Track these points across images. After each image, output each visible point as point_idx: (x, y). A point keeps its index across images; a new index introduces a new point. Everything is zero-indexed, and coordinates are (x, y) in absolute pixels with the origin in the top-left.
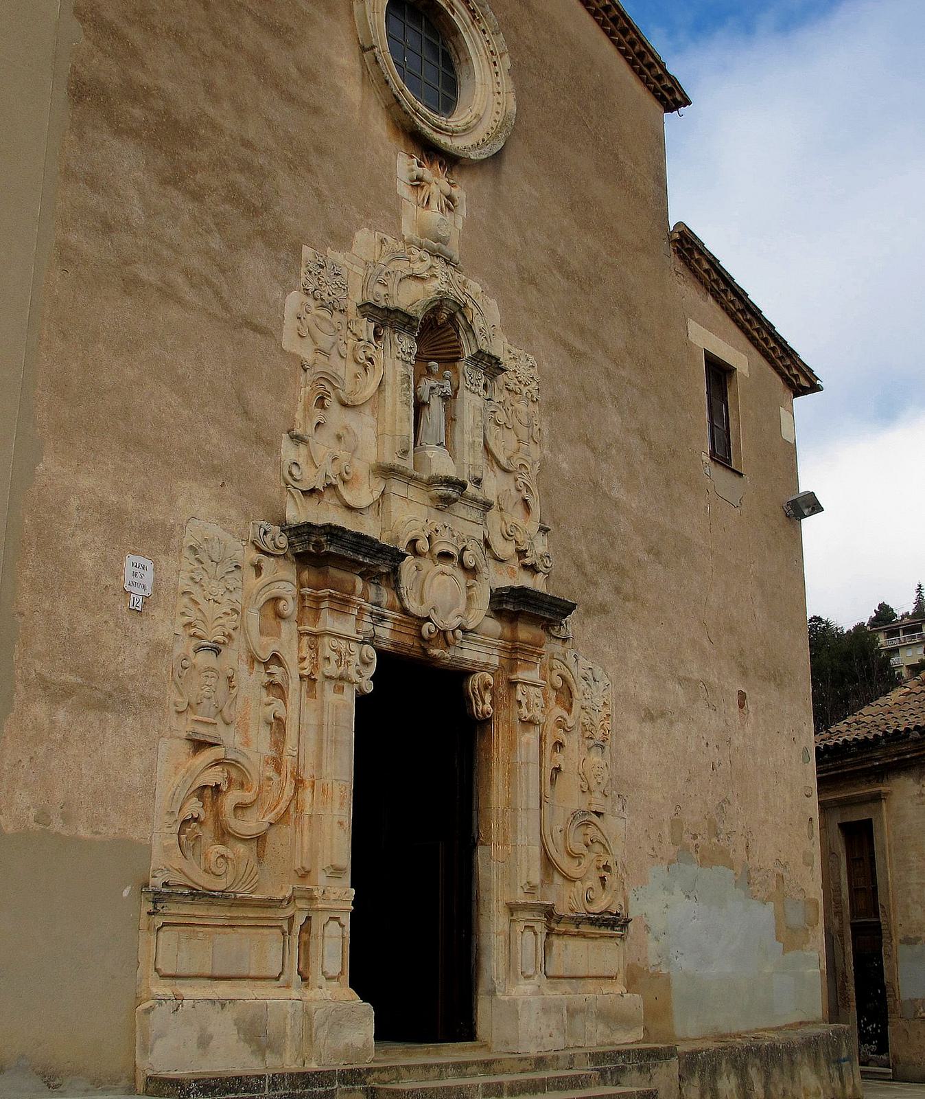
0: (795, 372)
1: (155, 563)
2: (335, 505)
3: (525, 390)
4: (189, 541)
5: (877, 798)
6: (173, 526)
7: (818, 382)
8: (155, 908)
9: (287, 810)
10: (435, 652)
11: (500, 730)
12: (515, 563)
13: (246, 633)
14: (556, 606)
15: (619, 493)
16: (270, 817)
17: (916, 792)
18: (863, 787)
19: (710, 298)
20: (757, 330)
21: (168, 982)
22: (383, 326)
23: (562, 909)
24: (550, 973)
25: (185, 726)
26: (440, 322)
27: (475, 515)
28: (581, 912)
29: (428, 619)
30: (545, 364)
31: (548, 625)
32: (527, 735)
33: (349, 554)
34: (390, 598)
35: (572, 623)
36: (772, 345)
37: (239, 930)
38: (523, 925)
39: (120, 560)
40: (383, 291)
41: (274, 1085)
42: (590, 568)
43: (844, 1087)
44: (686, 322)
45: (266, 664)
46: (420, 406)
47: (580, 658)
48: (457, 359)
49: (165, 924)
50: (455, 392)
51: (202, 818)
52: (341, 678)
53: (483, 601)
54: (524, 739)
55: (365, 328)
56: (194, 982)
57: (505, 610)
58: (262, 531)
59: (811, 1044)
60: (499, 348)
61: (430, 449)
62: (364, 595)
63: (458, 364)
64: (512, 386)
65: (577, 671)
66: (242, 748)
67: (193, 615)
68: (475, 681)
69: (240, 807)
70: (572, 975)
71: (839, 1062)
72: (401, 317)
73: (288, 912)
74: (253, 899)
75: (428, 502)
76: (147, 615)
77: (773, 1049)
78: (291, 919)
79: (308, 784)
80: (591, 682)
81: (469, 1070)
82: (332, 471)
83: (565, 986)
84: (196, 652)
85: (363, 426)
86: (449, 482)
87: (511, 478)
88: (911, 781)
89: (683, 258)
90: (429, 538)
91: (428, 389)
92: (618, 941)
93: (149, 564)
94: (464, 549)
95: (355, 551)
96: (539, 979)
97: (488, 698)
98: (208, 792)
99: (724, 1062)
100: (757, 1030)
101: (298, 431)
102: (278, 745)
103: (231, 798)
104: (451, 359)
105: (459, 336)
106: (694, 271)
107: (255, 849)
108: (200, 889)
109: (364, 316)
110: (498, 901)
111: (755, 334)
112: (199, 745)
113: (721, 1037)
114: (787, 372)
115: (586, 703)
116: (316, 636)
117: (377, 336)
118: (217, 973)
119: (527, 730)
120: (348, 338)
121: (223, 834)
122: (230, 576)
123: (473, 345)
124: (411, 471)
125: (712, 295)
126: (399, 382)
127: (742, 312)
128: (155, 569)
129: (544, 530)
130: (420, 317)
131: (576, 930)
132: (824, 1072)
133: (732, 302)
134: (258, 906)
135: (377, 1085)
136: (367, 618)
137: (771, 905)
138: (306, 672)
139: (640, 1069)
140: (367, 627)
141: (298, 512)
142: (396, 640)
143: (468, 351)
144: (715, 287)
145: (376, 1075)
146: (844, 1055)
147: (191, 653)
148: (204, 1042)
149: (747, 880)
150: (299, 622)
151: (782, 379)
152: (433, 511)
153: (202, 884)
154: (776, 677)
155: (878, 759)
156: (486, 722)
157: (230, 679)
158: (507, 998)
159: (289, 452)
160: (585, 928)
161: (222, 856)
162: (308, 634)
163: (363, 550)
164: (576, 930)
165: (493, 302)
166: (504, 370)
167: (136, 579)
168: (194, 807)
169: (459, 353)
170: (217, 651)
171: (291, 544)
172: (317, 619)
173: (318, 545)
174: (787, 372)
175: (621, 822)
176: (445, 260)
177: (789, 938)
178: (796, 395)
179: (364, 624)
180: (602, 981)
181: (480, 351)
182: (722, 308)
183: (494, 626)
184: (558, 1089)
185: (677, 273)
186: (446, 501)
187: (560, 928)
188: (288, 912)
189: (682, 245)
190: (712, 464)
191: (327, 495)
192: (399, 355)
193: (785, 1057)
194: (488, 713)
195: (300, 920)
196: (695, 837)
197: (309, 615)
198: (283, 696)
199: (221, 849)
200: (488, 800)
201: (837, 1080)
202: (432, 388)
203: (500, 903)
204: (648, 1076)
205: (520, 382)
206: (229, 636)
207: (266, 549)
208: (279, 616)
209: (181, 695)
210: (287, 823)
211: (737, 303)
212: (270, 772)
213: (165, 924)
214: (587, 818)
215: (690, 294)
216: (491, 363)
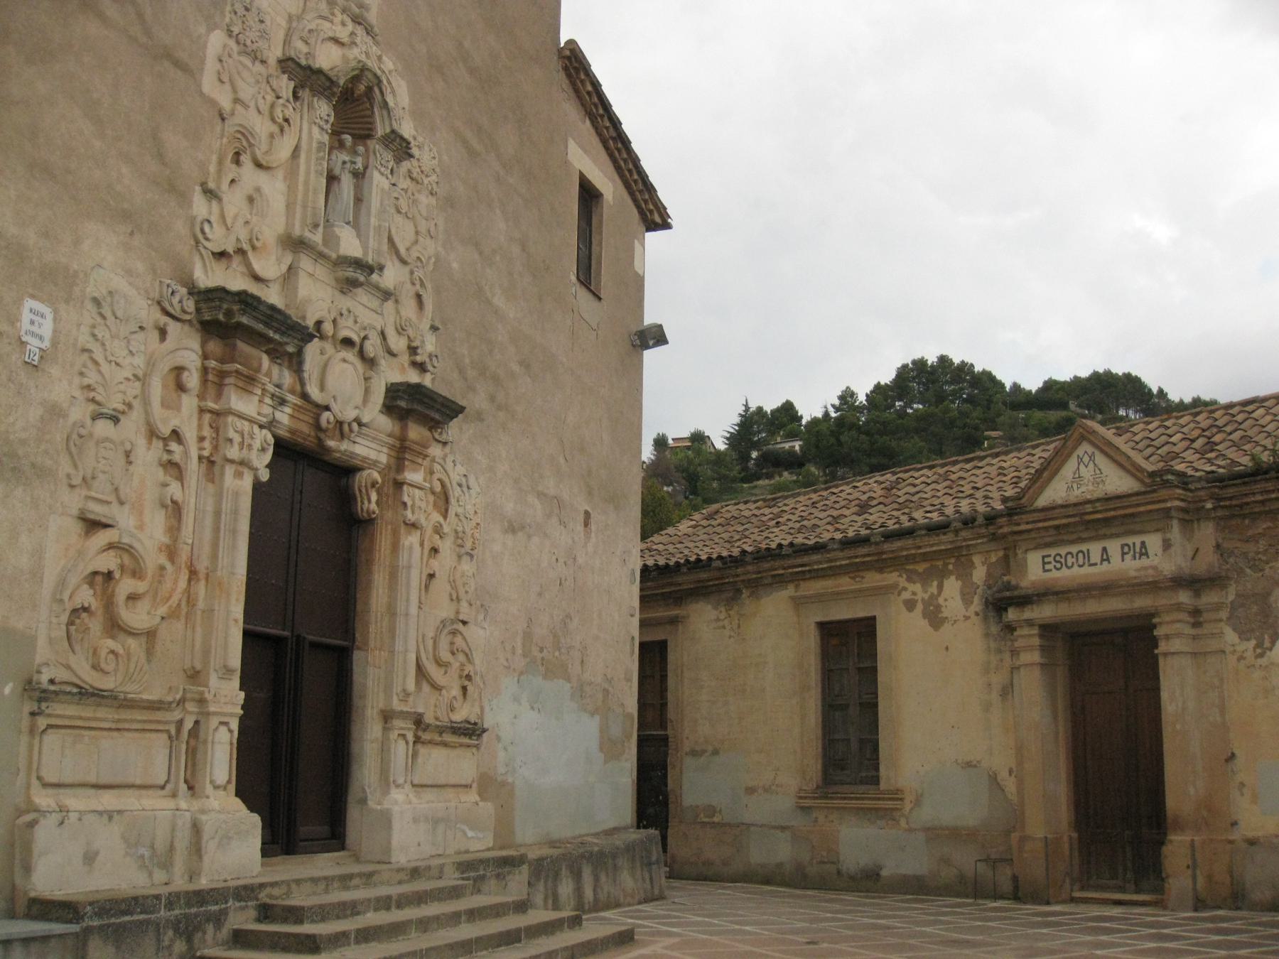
0: (651, 207)
1: (56, 312)
2: (243, 273)
3: (426, 181)
4: (91, 290)
5: (674, 621)
6: (76, 272)
7: (669, 220)
8: (39, 708)
9: (179, 605)
10: (331, 443)
11: (384, 531)
12: (405, 359)
13: (146, 402)
14: (447, 407)
15: (499, 301)
16: (162, 610)
17: (713, 617)
18: (661, 609)
19: (588, 122)
20: (625, 161)
21: (50, 791)
22: (303, 87)
23: (428, 718)
24: (416, 782)
25: (74, 502)
26: (357, 93)
27: (375, 303)
28: (445, 721)
29: (327, 408)
30: (445, 157)
31: (434, 425)
32: (410, 538)
33: (260, 327)
34: (292, 381)
35: (454, 430)
36: (636, 177)
37: (126, 734)
38: (396, 732)
39: (19, 302)
40: (304, 49)
41: (170, 905)
42: (471, 373)
43: (652, 887)
44: (567, 141)
45: (165, 440)
46: (332, 179)
47: (458, 464)
48: (369, 137)
49: (50, 726)
50: (366, 168)
51: (93, 608)
52: (242, 463)
53: (378, 397)
54: (407, 543)
55: (285, 85)
56: (80, 791)
57: (398, 407)
58: (170, 290)
59: (630, 849)
60: (407, 130)
61: (337, 226)
62: (269, 374)
63: (369, 142)
64: (415, 175)
65: (456, 473)
66: (135, 531)
67: (93, 377)
68: (362, 478)
69: (133, 598)
70: (434, 783)
71: (650, 864)
72: (323, 79)
73: (177, 715)
74: (142, 701)
75: (333, 283)
76: (43, 370)
77: (601, 854)
78: (180, 723)
79: (202, 576)
80: (465, 489)
81: (356, 881)
82: (243, 235)
83: (429, 795)
84: (93, 419)
85: (274, 188)
86: (358, 264)
87: (407, 269)
88: (709, 607)
89: (569, 76)
90: (334, 321)
91: (339, 164)
92: (474, 750)
93: (47, 310)
94: (365, 338)
95: (266, 324)
96: (408, 787)
97: (374, 497)
98: (99, 579)
99: (564, 867)
100: (580, 836)
101: (211, 185)
102: (174, 529)
103: (126, 586)
104: (364, 136)
105: (373, 113)
106: (577, 91)
107: (144, 645)
108: (88, 687)
109: (284, 72)
110: (372, 707)
111: (622, 163)
112: (93, 525)
113: (552, 844)
114: (644, 206)
115: (460, 510)
116: (217, 414)
117: (296, 96)
118: (103, 781)
119: (410, 533)
120: (267, 93)
121: (113, 626)
122: (134, 336)
123: (387, 123)
124: (321, 248)
125: (590, 118)
126: (314, 150)
127: (613, 139)
128: (55, 319)
129: (434, 328)
130: (342, 82)
131: (440, 739)
132: (639, 872)
133: (607, 128)
134: (144, 708)
135: (268, 901)
136: (268, 400)
137: (597, 718)
138: (206, 453)
139: (498, 876)
140: (267, 410)
141: (208, 276)
142: (293, 426)
143: (380, 131)
144: (594, 110)
145: (268, 890)
146: (654, 858)
147: (88, 421)
148: (90, 858)
149: (580, 692)
150: (201, 397)
151: (639, 212)
152: (337, 293)
153: (90, 682)
154: (614, 500)
155: (686, 580)
156: (370, 521)
157: (128, 454)
158: (379, 807)
159: (200, 207)
160: (448, 738)
161: (112, 652)
162: (210, 412)
163: (275, 324)
164: (440, 739)
165: (403, 84)
166: (411, 156)
167: (35, 329)
168: (86, 596)
169: (371, 129)
170: (115, 420)
171: (198, 310)
172: (219, 395)
173: (229, 313)
174: (644, 206)
175: (481, 632)
176: (366, 29)
177: (609, 748)
178: (649, 230)
179: (265, 406)
180: (460, 790)
181: (393, 131)
182: (597, 133)
183: (386, 423)
184: (438, 900)
185: (563, 90)
186: (354, 283)
187: (426, 736)
188: (177, 715)
189: (571, 62)
190: (578, 285)
191: (237, 260)
192: (317, 121)
193: (610, 861)
194: (374, 513)
195: (189, 724)
196: (541, 650)
197: (212, 391)
198: (180, 477)
199: (110, 643)
200: (367, 603)
201: (648, 881)
202: (344, 163)
203: (375, 711)
204: (504, 883)
205: (422, 172)
206: (130, 406)
207: (173, 312)
208: (181, 388)
209: (76, 466)
210: (178, 618)
211: (611, 130)
212: (163, 560)
213: (50, 726)
214: (455, 626)
215: (571, 111)
216: (400, 145)
